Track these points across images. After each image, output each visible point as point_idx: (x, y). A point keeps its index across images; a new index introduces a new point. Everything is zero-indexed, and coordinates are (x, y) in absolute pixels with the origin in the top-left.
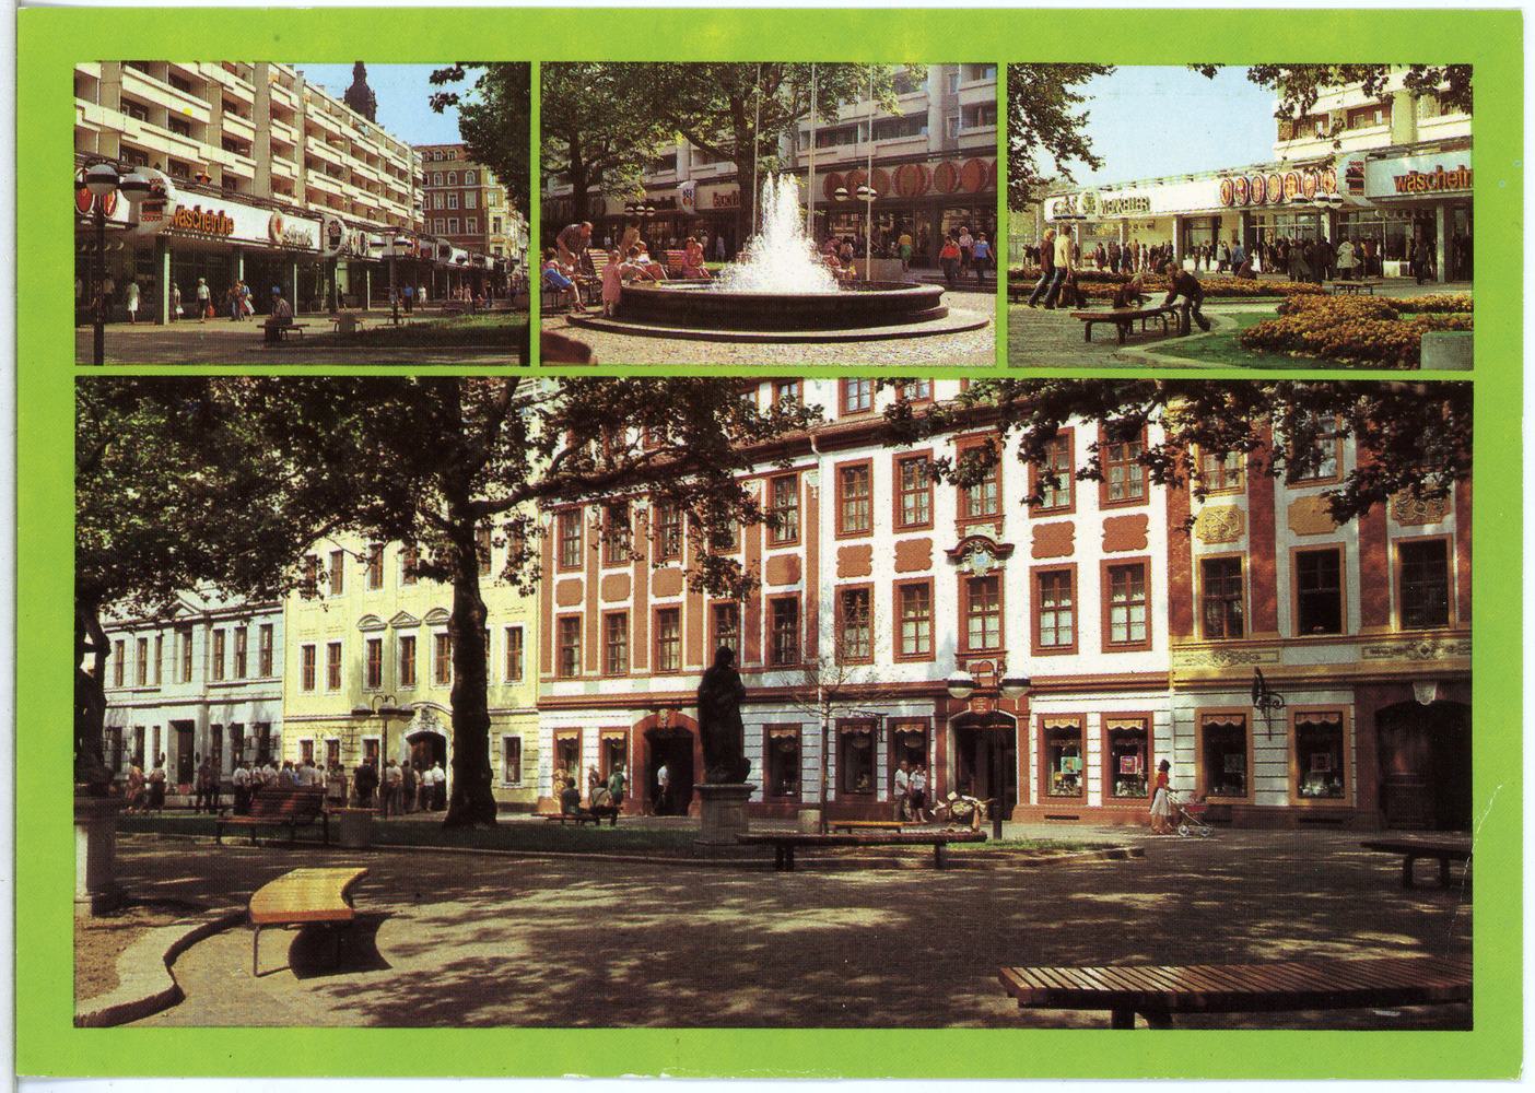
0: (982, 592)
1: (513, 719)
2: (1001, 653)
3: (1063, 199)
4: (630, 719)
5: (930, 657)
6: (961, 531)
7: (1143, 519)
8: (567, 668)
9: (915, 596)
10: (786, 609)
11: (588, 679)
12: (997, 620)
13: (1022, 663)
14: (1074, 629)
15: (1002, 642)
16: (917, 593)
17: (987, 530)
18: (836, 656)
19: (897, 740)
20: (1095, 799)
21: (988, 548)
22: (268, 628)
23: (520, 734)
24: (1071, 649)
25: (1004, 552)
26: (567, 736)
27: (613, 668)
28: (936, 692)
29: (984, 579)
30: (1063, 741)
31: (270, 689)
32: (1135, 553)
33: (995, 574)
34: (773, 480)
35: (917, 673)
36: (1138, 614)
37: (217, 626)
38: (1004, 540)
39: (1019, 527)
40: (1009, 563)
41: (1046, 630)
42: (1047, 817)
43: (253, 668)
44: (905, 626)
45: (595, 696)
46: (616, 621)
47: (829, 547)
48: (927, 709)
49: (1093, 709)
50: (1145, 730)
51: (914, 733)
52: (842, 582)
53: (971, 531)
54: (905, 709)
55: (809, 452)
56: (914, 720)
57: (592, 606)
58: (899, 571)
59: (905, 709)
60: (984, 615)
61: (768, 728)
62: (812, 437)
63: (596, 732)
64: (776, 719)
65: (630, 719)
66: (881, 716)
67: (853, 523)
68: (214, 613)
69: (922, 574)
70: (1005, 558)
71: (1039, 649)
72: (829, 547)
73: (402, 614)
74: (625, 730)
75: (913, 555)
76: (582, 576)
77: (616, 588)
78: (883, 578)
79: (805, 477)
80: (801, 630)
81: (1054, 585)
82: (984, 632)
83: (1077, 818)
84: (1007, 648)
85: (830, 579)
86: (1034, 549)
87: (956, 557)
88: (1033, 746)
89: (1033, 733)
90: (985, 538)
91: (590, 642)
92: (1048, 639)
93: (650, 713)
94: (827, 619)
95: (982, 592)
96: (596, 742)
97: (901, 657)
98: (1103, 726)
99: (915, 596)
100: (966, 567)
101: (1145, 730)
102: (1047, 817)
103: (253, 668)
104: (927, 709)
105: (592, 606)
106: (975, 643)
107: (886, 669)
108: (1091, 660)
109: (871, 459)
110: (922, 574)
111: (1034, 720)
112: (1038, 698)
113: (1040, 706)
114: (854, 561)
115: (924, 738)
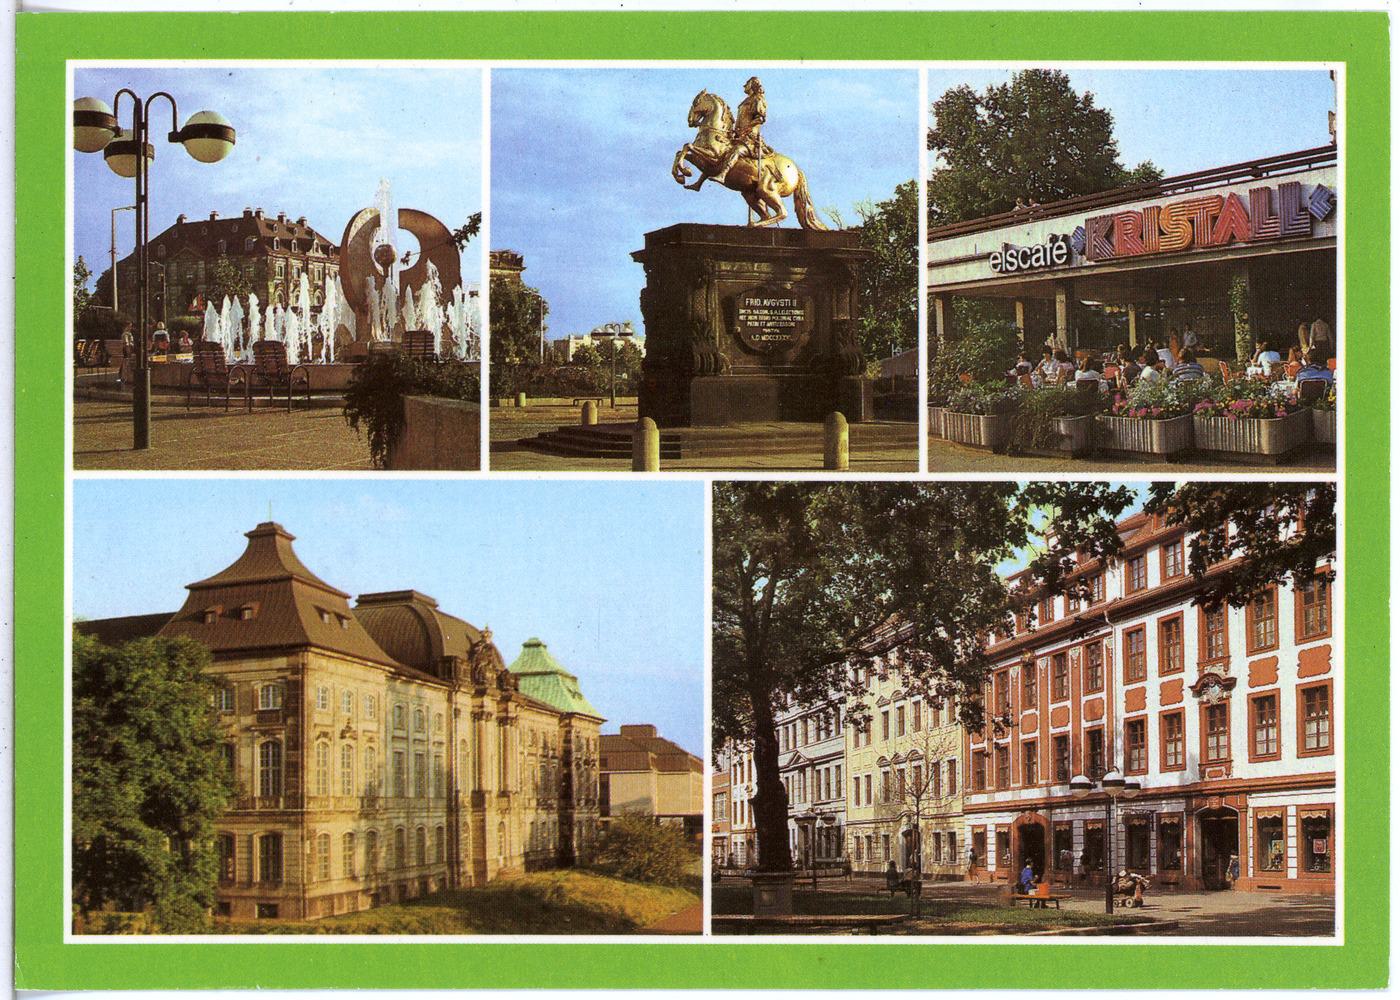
0: (1216, 717)
1: (951, 820)
2: (1228, 762)
3: (336, 913)
4: (1009, 818)
5: (1182, 767)
6: (1201, 671)
7: (1328, 649)
8: (980, 786)
9: (1173, 722)
10: (1095, 736)
11: (1014, 789)
12: (662, 819)
13: (1243, 769)
14: (1278, 741)
15: (1229, 754)
16: (1318, 695)
17: (1218, 670)
18: (1125, 769)
19: (1162, 828)
20: (1292, 874)
21: (1218, 682)
22: (838, 767)
23: (955, 830)
24: (1276, 757)
25: (1229, 684)
26: (979, 830)
27: (1003, 785)
28: (1184, 793)
29: (1217, 706)
30: (1271, 828)
31: (839, 805)
32: (1270, 687)
33: (1223, 702)
34: (1055, 657)
35: (1172, 780)
36: (1324, 726)
37: (817, 768)
38: (1231, 674)
39: (1240, 665)
40: (1234, 692)
41: (1311, 736)
42: (1259, 887)
43: (833, 794)
44: (1308, 726)
45: (992, 803)
46: (1030, 746)
47: (1120, 689)
48: (1178, 806)
49: (1291, 801)
50: (1328, 818)
51: (1172, 824)
52: (1164, 708)
53: (1208, 670)
54: (1165, 807)
55: (1104, 624)
56: (1171, 815)
57: (1044, 732)
58: (1127, 712)
59: (1165, 807)
60: (1318, 719)
61: (1085, 822)
62: (1105, 613)
63: (993, 828)
64: (1091, 816)
65: (1009, 818)
66: (1152, 812)
67: (1135, 670)
68: (817, 759)
69: (1141, 712)
70: (1230, 690)
71: (1255, 758)
72: (1120, 689)
73: (914, 752)
74: (1009, 825)
75: (1171, 692)
76: (1068, 703)
77: (1060, 718)
78: (1153, 711)
79: (1105, 641)
80: (1053, 763)
81: (1264, 707)
82: (1268, 740)
83: (1279, 888)
84: (1232, 758)
85: (1121, 714)
86: (1126, 706)
87: (1199, 690)
88: (1250, 832)
89: (1250, 823)
90: (1216, 675)
91: (991, 767)
92: (1261, 750)
93: (1020, 814)
94: (1119, 743)
95: (1216, 717)
96: (1081, 832)
97: (1165, 768)
98: (1297, 815)
99: (1173, 722)
100: (1205, 698)
101: (1328, 818)
102: (1259, 887)
103: (833, 794)
104: (1178, 806)
105: (1044, 732)
106: (1213, 756)
107: (1156, 779)
108: (1290, 764)
109: (1145, 623)
110: (1141, 712)
111: (1250, 813)
112: (1254, 795)
113: (1256, 801)
114: (1136, 699)
115: (1178, 827)
